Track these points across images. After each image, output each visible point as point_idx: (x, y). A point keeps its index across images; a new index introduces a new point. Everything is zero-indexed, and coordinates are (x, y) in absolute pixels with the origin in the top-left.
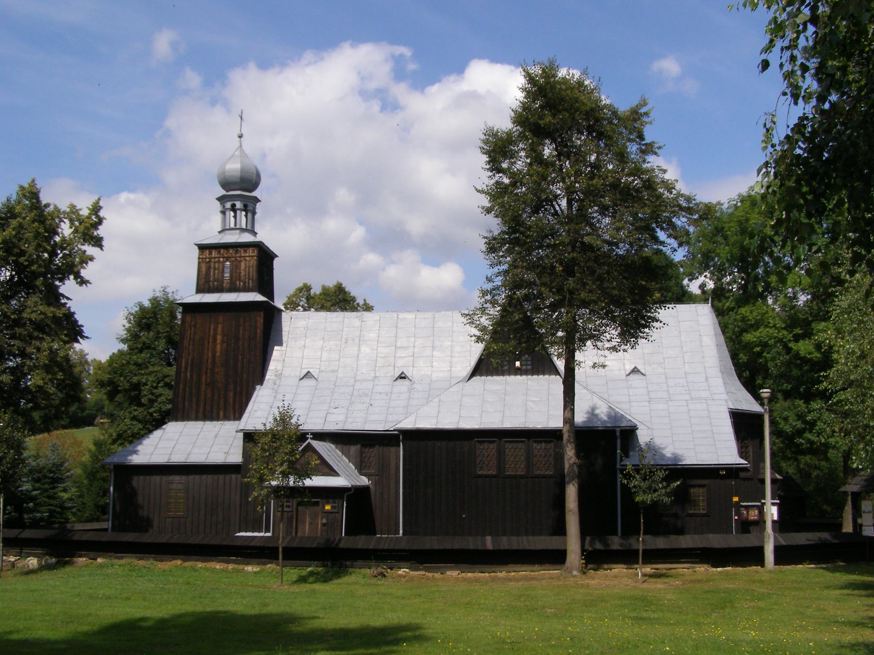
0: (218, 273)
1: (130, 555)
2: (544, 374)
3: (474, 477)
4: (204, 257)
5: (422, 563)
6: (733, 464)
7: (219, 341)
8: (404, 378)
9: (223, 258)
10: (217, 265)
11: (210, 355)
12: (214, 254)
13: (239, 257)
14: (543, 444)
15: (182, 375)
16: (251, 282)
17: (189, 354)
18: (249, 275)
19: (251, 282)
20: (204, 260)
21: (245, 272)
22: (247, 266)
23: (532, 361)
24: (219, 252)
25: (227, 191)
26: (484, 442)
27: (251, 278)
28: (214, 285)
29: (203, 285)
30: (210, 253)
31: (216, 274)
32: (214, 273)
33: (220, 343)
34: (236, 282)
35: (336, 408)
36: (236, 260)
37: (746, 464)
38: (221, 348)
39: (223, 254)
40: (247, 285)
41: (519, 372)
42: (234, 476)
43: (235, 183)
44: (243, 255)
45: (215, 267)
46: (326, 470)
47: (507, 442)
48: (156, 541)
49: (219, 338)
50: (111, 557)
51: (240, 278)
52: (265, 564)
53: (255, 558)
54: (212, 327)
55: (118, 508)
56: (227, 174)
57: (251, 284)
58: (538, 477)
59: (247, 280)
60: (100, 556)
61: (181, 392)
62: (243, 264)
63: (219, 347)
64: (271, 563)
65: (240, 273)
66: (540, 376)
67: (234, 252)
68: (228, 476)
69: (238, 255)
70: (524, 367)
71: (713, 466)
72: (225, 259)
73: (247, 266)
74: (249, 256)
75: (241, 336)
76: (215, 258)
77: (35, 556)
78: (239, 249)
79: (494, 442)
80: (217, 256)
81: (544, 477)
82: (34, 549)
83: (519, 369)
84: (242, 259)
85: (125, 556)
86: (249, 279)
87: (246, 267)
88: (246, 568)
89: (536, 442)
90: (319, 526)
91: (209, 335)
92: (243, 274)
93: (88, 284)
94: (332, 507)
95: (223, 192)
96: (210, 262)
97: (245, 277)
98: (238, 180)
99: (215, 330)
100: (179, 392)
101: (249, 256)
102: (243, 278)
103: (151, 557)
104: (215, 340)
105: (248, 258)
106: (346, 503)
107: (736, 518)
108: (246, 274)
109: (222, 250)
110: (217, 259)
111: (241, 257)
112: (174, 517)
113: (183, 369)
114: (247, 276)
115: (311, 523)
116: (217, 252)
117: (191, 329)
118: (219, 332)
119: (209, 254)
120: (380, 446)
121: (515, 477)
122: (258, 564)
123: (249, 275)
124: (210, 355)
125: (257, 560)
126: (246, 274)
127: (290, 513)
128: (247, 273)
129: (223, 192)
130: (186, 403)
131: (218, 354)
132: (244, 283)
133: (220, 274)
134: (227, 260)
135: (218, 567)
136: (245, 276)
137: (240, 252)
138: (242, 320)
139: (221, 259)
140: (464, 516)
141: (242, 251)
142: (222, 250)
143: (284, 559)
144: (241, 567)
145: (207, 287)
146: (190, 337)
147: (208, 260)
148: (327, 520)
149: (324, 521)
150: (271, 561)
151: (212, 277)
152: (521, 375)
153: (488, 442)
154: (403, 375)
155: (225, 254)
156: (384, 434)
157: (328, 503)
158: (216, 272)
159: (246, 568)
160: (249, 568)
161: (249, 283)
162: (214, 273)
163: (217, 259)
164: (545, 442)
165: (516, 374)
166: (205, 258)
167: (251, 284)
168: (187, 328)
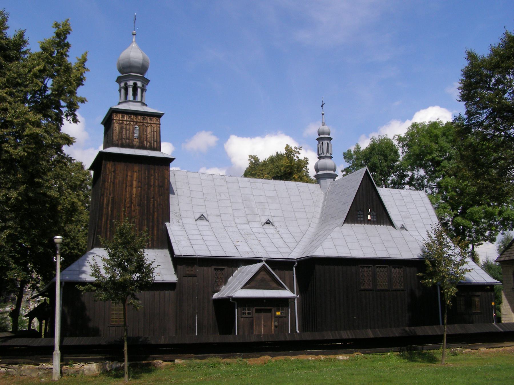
0: (129, 134)
1: (213, 355)
2: (383, 224)
3: (360, 291)
4: (118, 119)
5: (468, 343)
6: (494, 283)
7: (134, 186)
8: (269, 223)
9: (133, 122)
10: (128, 127)
11: (127, 196)
12: (126, 118)
13: (146, 123)
14: (397, 269)
15: (104, 210)
16: (155, 143)
17: (110, 195)
18: (154, 137)
19: (155, 143)
20: (118, 122)
21: (151, 135)
22: (153, 131)
23: (376, 215)
24: (130, 117)
25: (122, 74)
26: (364, 267)
27: (155, 140)
28: (126, 142)
29: (117, 140)
30: (123, 117)
31: (128, 133)
32: (126, 133)
33: (136, 188)
34: (143, 141)
35: (237, 242)
36: (143, 125)
37: (499, 283)
38: (136, 192)
39: (133, 119)
40: (153, 145)
41: (370, 222)
42: (167, 292)
43: (137, 67)
44: (149, 122)
45: (126, 127)
46: (275, 285)
47: (377, 267)
48: (224, 341)
49: (135, 183)
50: (191, 357)
51: (147, 139)
52: (352, 353)
53: (342, 349)
54: (129, 174)
55: (69, 321)
56: (132, 59)
57: (155, 145)
58: (396, 291)
59: (153, 141)
60: (177, 358)
61: (103, 222)
62: (149, 129)
63: (135, 190)
64: (357, 352)
65: (147, 135)
66: (378, 226)
67: (142, 119)
68: (162, 293)
69: (145, 121)
70: (372, 219)
71: (485, 284)
72: (135, 123)
73: (153, 131)
74: (154, 124)
75: (152, 184)
76: (126, 121)
77: (95, 361)
78: (146, 117)
79: (386, 267)
80: (128, 119)
81: (399, 290)
82: (83, 355)
83: (369, 220)
84: (148, 125)
85: (206, 356)
86: (154, 141)
87: (151, 131)
88: (337, 357)
89: (393, 267)
90: (273, 328)
91: (127, 180)
92: (149, 136)
93: (78, 123)
94: (281, 313)
95: (120, 75)
96: (122, 123)
97: (151, 139)
98: (140, 66)
99: (132, 177)
100: (102, 223)
101: (154, 124)
102: (149, 139)
103: (237, 355)
104: (131, 185)
105: (153, 125)
106: (290, 310)
107: (495, 315)
108: (151, 136)
109: (132, 116)
110: (128, 122)
111: (147, 123)
112: (117, 326)
113: (105, 206)
114: (152, 139)
115: (265, 326)
116: (128, 117)
117: (111, 174)
118: (135, 179)
119: (122, 118)
120: (279, 270)
121: (383, 290)
122: (345, 353)
123: (154, 137)
124: (127, 196)
125: (344, 350)
126: (151, 136)
127: (251, 318)
128: (152, 136)
129: (120, 75)
130: (108, 233)
131: (134, 196)
132: (150, 144)
133: (131, 134)
134: (136, 124)
135: (310, 358)
136: (151, 137)
137: (147, 119)
138: (152, 172)
139: (132, 123)
140: (355, 317)
141: (149, 119)
142: (132, 116)
143: (447, 342)
144: (332, 357)
145: (120, 143)
146: (111, 181)
147: (121, 122)
148: (278, 323)
149: (276, 324)
150: (357, 350)
151: (124, 135)
152: (371, 224)
153: (367, 267)
154: (268, 222)
155: (134, 119)
156: (285, 261)
157: (278, 310)
158: (128, 132)
159: (337, 357)
160: (341, 357)
161: (154, 144)
162: (126, 133)
163: (128, 122)
164: (398, 268)
165: (368, 224)
166: (119, 120)
167: (155, 145)
168: (108, 173)
